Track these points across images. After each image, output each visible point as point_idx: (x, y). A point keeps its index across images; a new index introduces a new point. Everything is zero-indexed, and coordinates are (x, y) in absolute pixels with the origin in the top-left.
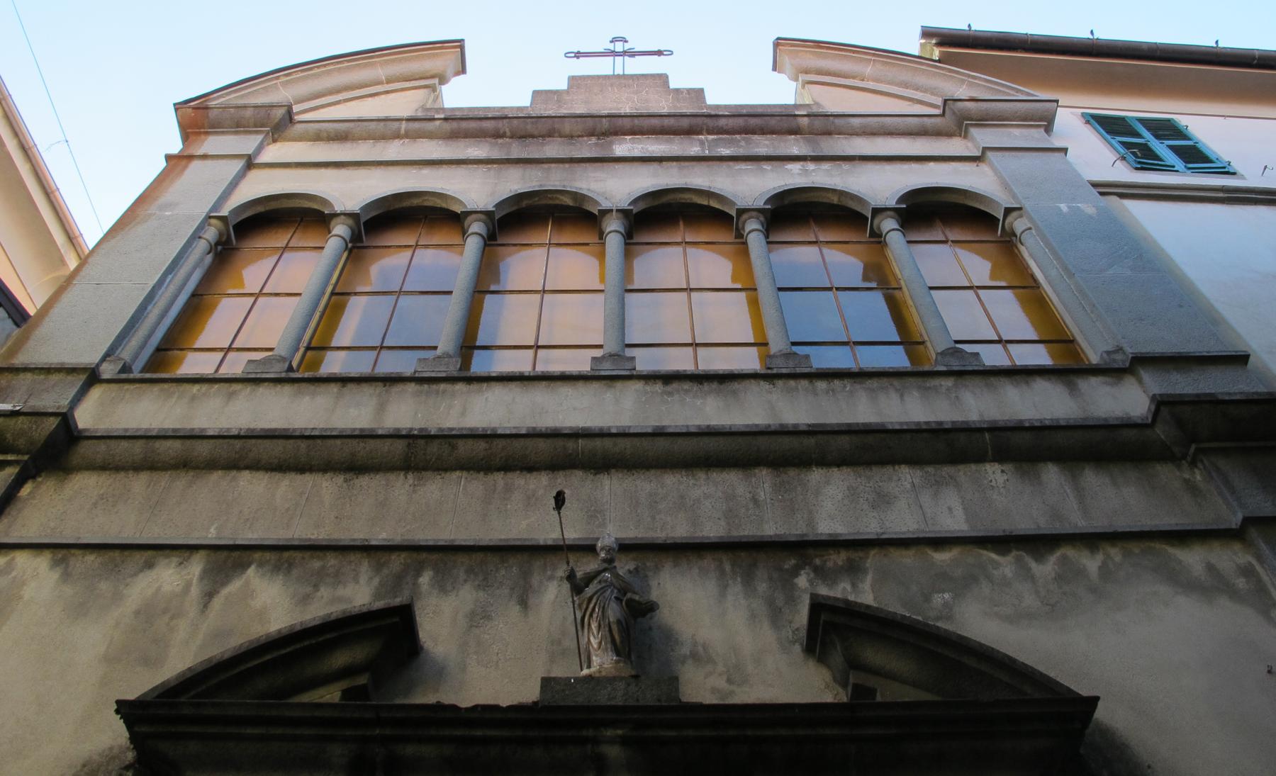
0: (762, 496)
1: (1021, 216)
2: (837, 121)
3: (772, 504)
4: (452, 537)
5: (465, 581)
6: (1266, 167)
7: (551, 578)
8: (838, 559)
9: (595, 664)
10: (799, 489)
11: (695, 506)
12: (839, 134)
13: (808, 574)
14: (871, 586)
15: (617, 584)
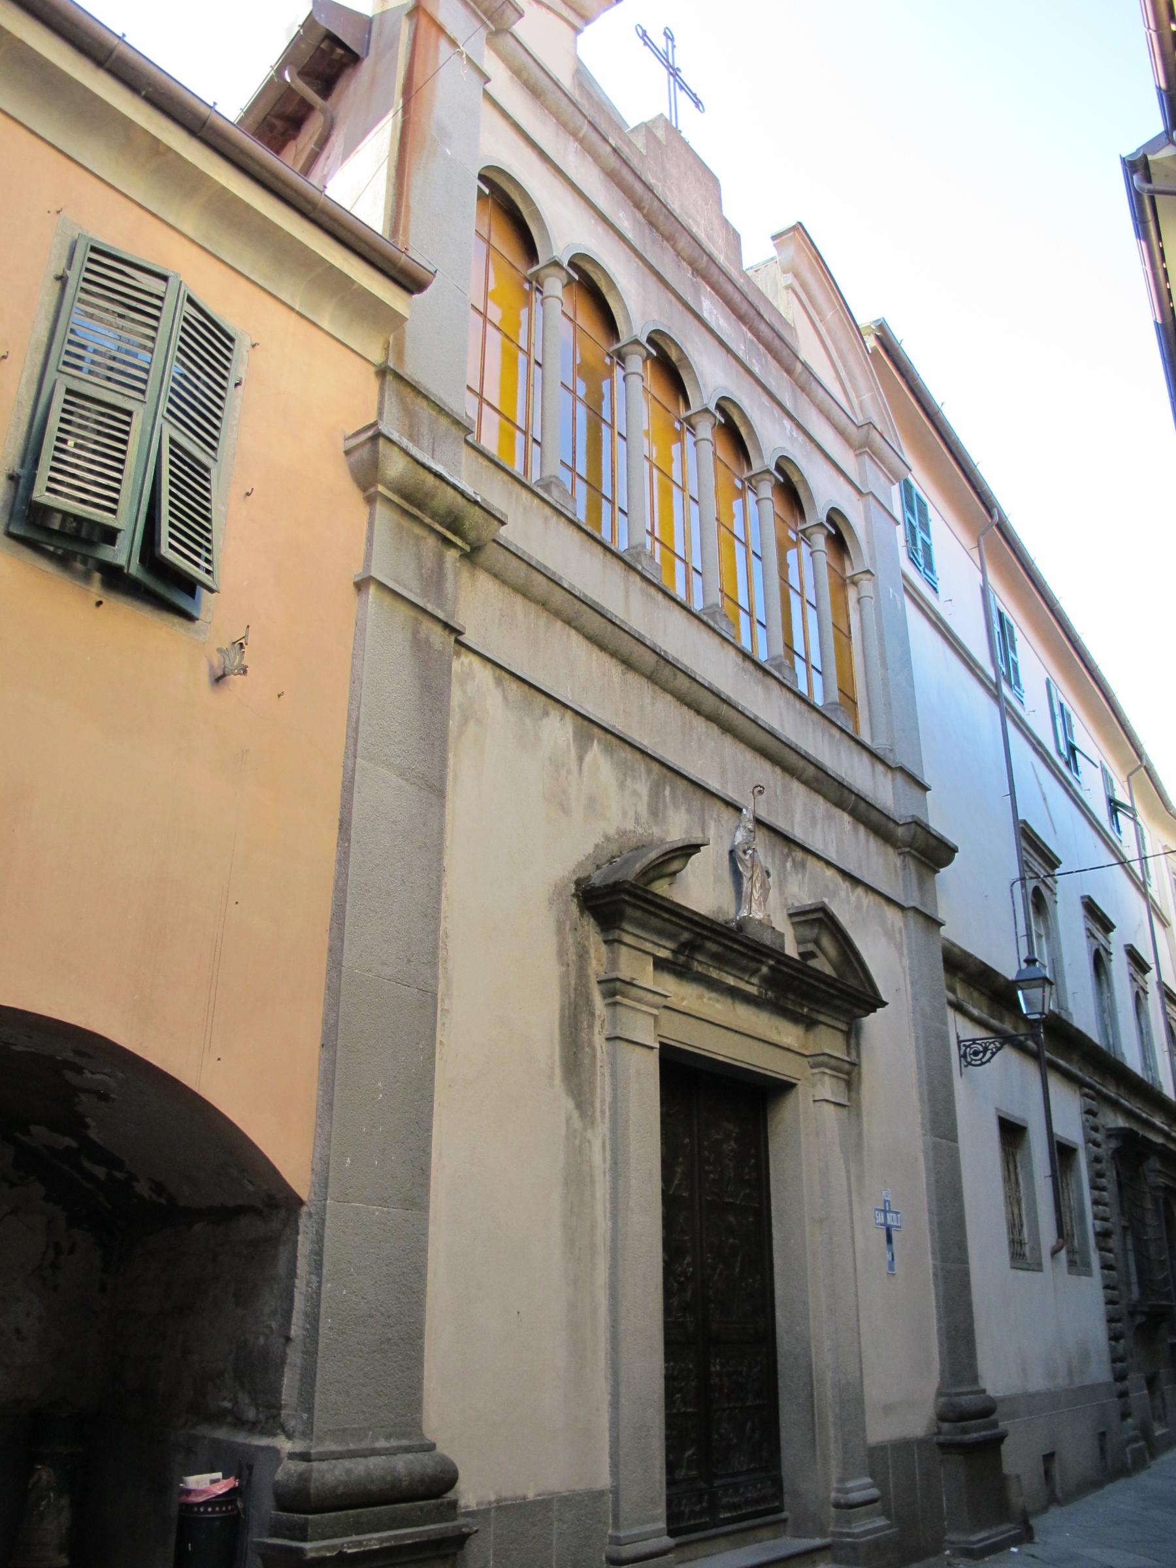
1: (870, 580)
2: (814, 384)
6: (951, 600)
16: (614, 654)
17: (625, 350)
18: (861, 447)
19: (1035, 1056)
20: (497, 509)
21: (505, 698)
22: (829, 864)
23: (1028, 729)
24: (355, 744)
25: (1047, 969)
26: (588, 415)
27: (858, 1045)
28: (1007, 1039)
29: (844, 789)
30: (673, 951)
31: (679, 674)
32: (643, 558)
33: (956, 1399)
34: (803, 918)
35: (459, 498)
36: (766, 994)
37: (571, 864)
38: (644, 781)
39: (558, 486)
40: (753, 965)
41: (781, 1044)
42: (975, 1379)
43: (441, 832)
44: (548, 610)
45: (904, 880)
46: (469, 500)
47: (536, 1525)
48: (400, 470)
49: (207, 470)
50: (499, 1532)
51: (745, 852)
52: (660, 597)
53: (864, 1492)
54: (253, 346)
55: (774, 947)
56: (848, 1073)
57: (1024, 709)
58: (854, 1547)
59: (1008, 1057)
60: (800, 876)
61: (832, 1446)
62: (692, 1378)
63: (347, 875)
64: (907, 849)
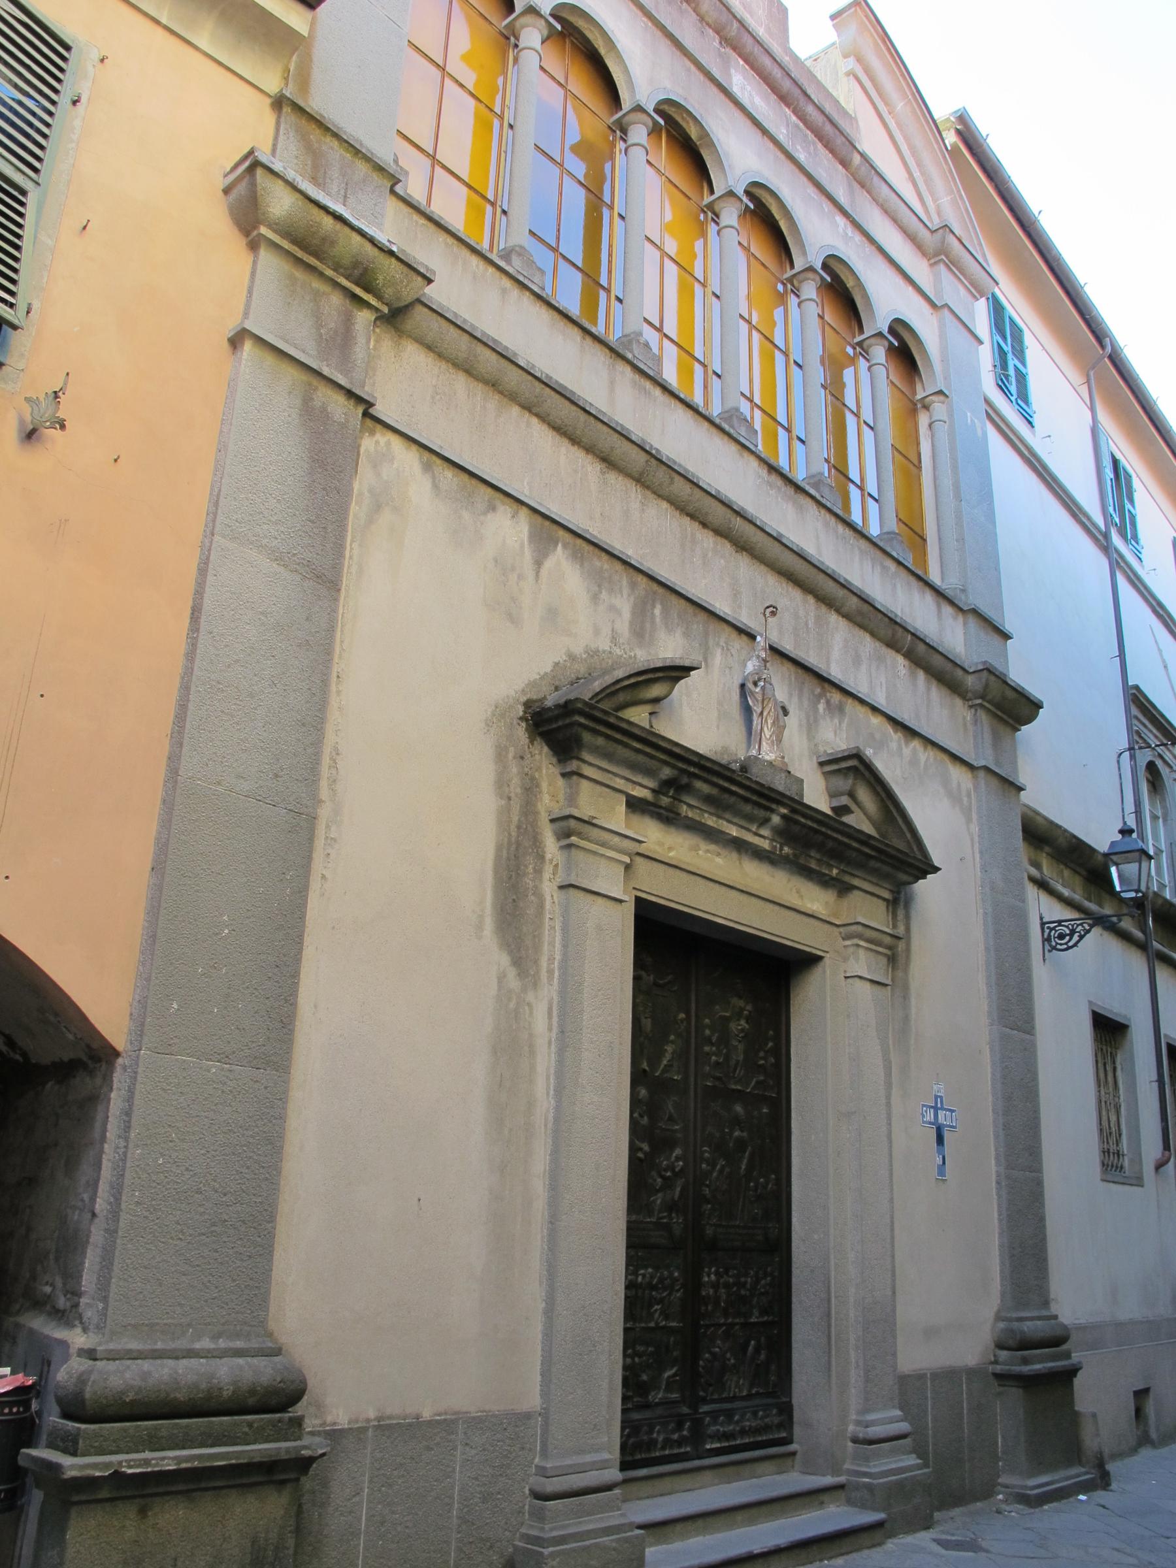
1: (943, 403)
2: (876, 179)
12: (868, 192)
16: (589, 449)
17: (627, 118)
18: (936, 254)
19: (1143, 947)
20: (422, 264)
21: (435, 486)
22: (875, 709)
23: (1146, 587)
24: (214, 521)
25: (1164, 854)
26: (587, 199)
27: (907, 917)
28: (1100, 921)
29: (897, 627)
30: (653, 791)
31: (677, 478)
32: (635, 346)
33: (1015, 1325)
34: (835, 767)
35: (368, 247)
36: (781, 849)
37: (520, 684)
38: (625, 596)
39: (519, 255)
40: (762, 813)
41: (802, 910)
42: (1046, 1303)
43: (331, 629)
44: (501, 393)
45: (975, 737)
46: (381, 249)
47: (432, 1449)
48: (286, 207)
49: (24, 193)
50: (379, 1455)
51: (755, 684)
52: (657, 392)
53: (888, 1427)
54: (102, 60)
55: (788, 793)
56: (890, 948)
57: (1143, 567)
58: (870, 1488)
59: (1096, 939)
60: (836, 721)
61: (853, 1372)
62: (677, 1288)
63: (192, 670)
64: (979, 701)
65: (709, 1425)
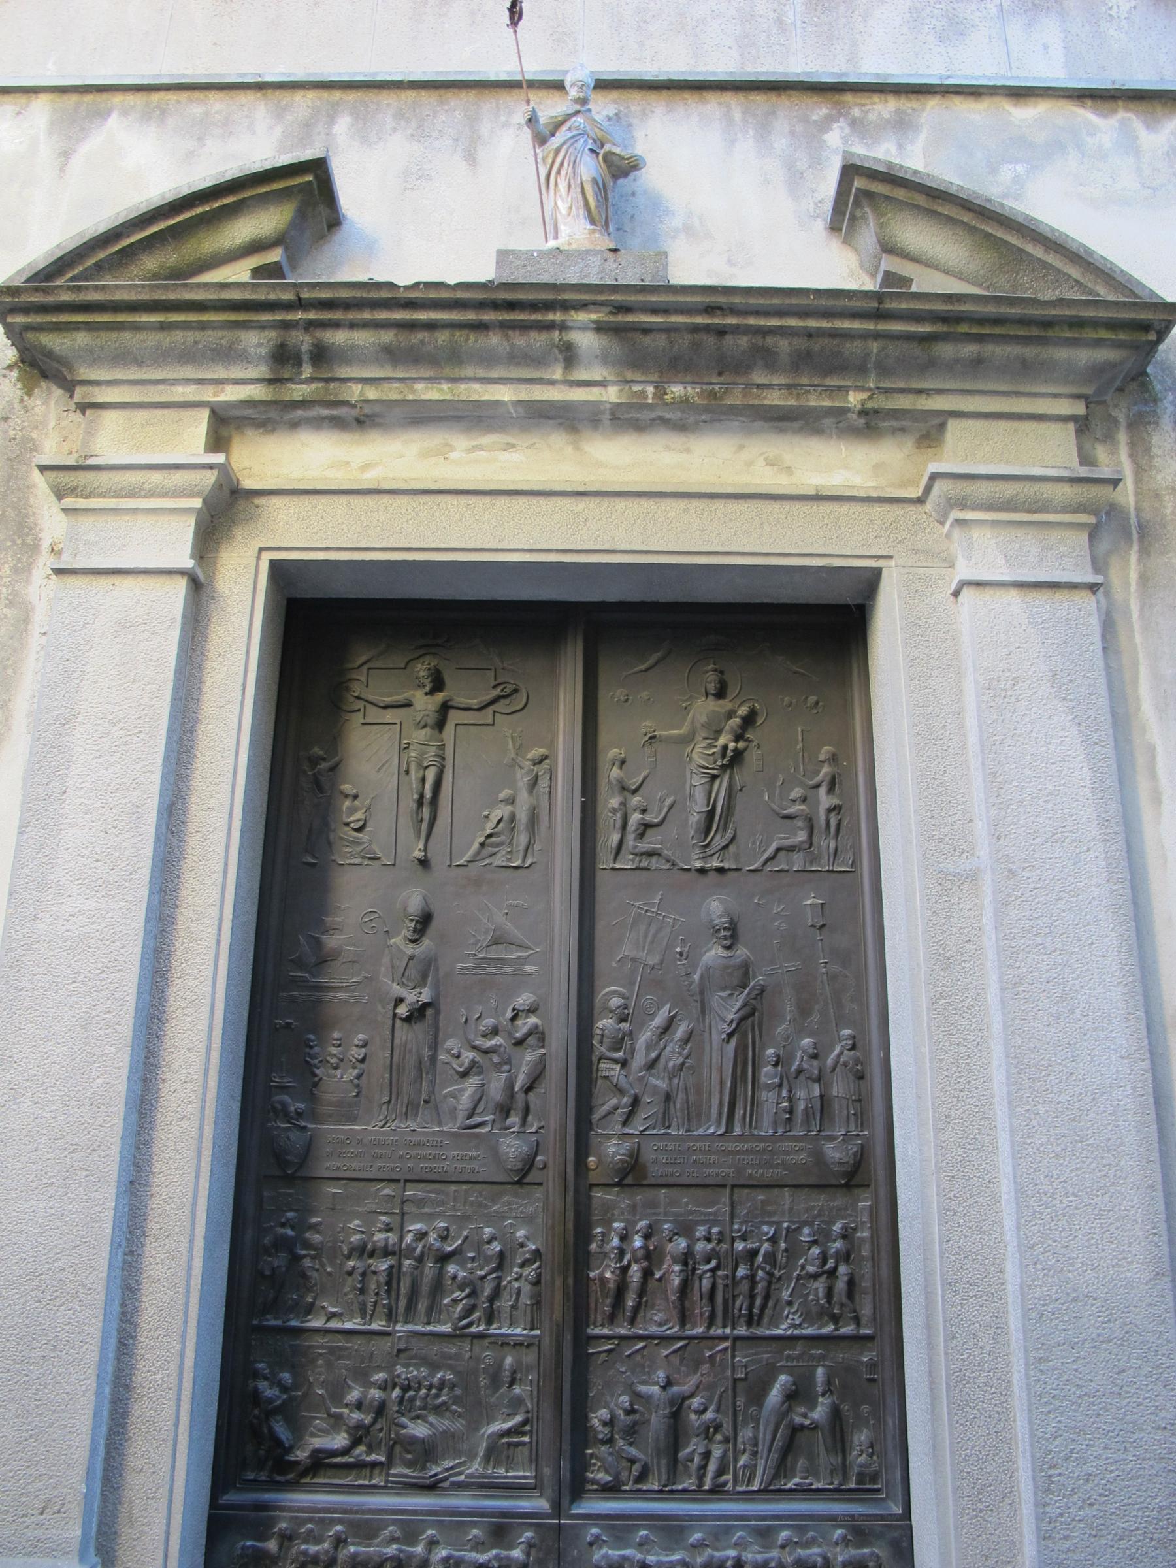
0: (790, 17)
3: (803, 28)
4: (373, 70)
5: (395, 129)
7: (505, 125)
8: (884, 108)
9: (563, 235)
10: (842, 8)
11: (698, 29)
13: (842, 128)
14: (923, 148)
15: (591, 134)
40: (538, 339)
65: (595, 1542)
